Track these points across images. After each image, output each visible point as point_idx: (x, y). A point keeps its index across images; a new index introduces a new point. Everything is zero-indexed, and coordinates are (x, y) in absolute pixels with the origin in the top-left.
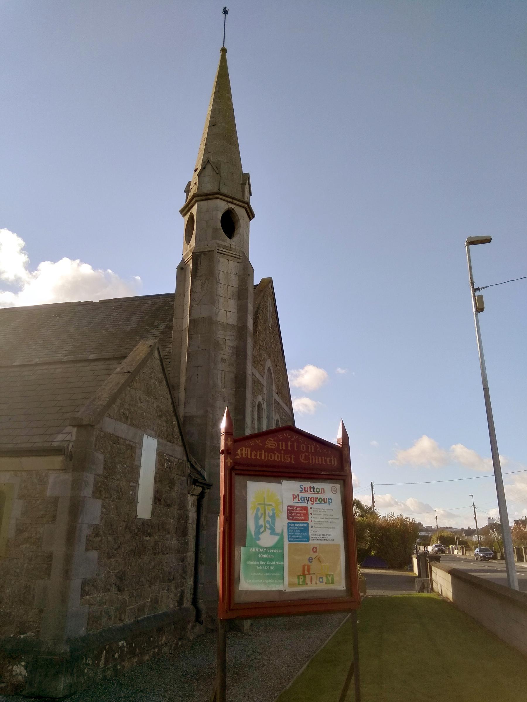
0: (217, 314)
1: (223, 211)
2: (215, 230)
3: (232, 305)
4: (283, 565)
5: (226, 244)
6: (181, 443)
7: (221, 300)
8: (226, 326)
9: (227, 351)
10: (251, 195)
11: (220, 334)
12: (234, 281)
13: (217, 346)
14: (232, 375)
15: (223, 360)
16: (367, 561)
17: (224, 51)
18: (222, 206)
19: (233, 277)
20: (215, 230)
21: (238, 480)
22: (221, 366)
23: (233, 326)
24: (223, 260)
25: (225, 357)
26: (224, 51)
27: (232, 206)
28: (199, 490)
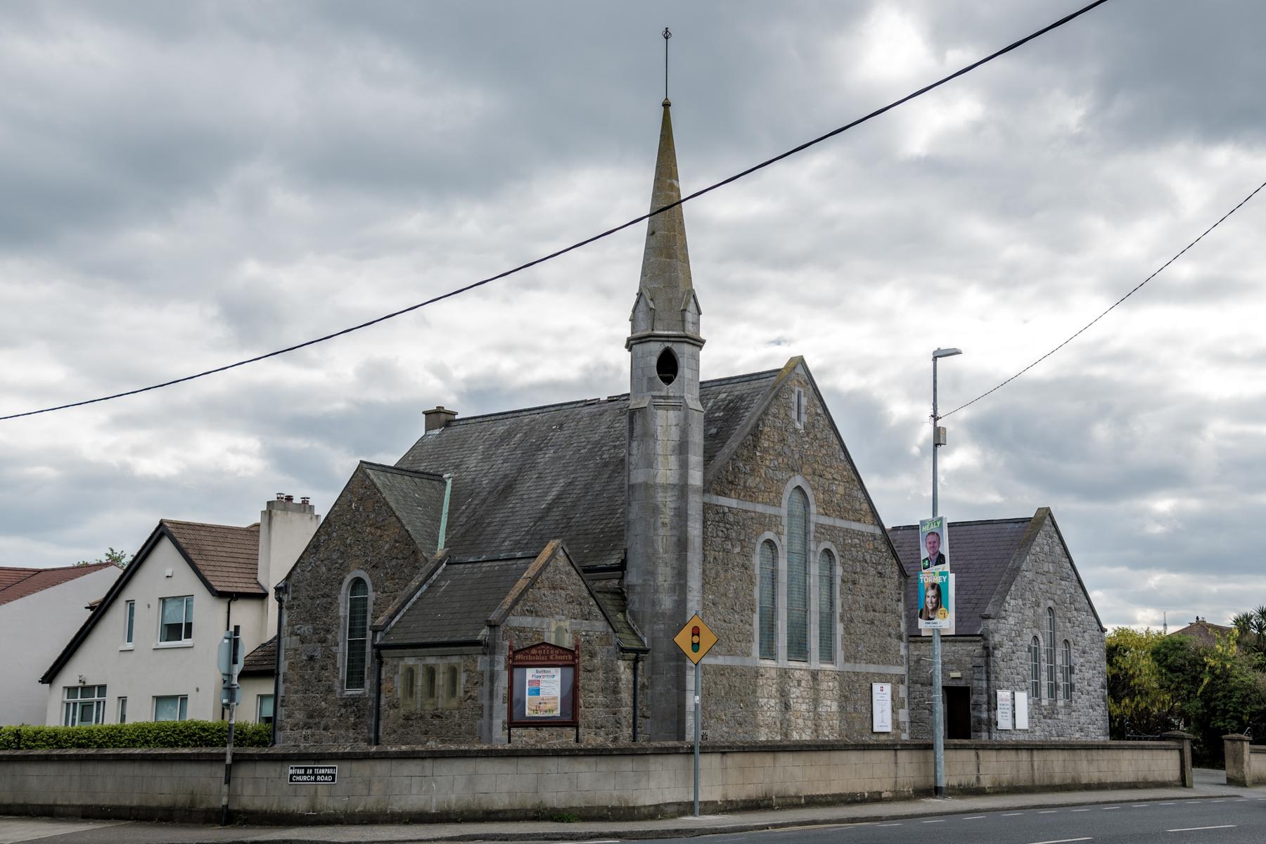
0: (655, 476)
1: (658, 354)
2: (651, 380)
3: (673, 461)
4: (366, 599)
5: (663, 394)
6: (603, 618)
7: (660, 459)
8: (665, 487)
9: (667, 515)
10: (700, 313)
11: (660, 497)
12: (674, 434)
13: (655, 510)
14: (674, 539)
15: (664, 524)
16: (681, 735)
17: (666, 105)
18: (657, 348)
19: (673, 428)
20: (651, 380)
21: (517, 672)
22: (662, 531)
23: (675, 485)
24: (660, 413)
25: (667, 521)
26: (666, 105)
27: (668, 345)
28: (633, 655)
